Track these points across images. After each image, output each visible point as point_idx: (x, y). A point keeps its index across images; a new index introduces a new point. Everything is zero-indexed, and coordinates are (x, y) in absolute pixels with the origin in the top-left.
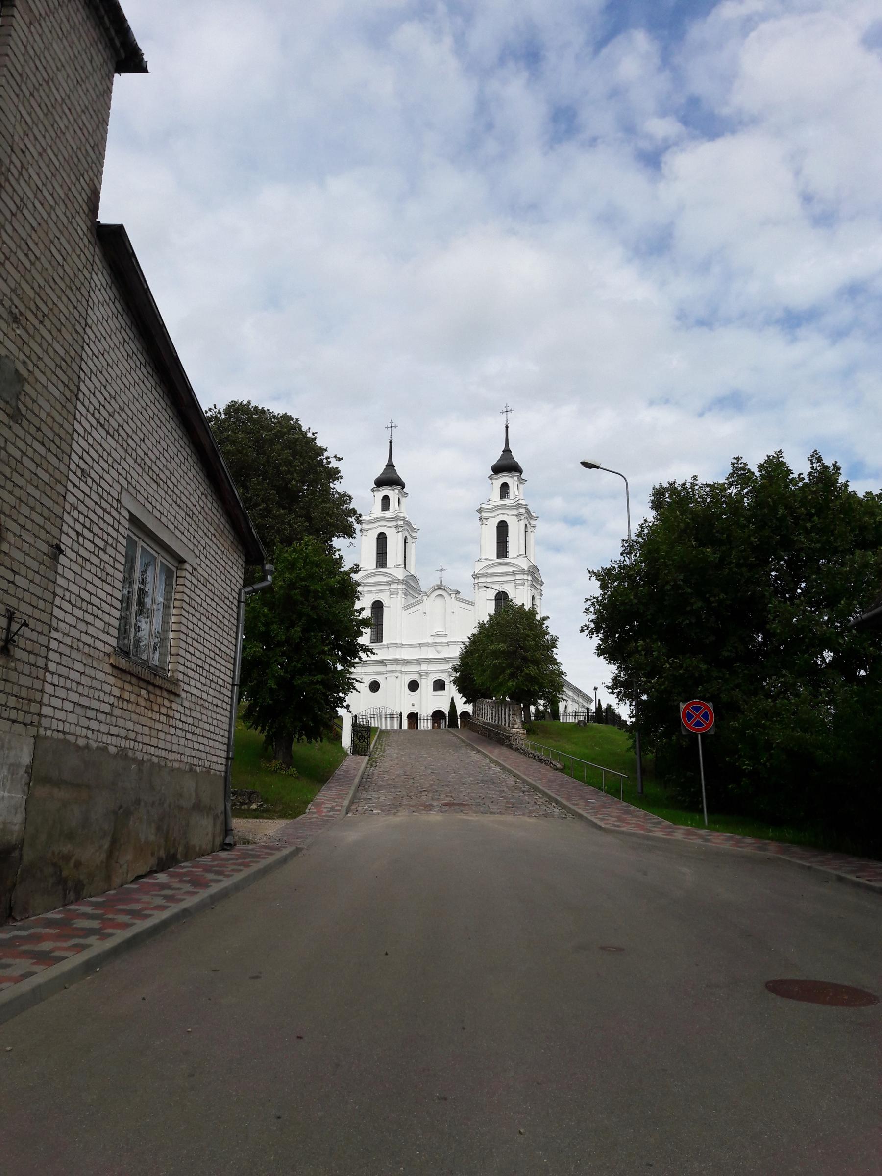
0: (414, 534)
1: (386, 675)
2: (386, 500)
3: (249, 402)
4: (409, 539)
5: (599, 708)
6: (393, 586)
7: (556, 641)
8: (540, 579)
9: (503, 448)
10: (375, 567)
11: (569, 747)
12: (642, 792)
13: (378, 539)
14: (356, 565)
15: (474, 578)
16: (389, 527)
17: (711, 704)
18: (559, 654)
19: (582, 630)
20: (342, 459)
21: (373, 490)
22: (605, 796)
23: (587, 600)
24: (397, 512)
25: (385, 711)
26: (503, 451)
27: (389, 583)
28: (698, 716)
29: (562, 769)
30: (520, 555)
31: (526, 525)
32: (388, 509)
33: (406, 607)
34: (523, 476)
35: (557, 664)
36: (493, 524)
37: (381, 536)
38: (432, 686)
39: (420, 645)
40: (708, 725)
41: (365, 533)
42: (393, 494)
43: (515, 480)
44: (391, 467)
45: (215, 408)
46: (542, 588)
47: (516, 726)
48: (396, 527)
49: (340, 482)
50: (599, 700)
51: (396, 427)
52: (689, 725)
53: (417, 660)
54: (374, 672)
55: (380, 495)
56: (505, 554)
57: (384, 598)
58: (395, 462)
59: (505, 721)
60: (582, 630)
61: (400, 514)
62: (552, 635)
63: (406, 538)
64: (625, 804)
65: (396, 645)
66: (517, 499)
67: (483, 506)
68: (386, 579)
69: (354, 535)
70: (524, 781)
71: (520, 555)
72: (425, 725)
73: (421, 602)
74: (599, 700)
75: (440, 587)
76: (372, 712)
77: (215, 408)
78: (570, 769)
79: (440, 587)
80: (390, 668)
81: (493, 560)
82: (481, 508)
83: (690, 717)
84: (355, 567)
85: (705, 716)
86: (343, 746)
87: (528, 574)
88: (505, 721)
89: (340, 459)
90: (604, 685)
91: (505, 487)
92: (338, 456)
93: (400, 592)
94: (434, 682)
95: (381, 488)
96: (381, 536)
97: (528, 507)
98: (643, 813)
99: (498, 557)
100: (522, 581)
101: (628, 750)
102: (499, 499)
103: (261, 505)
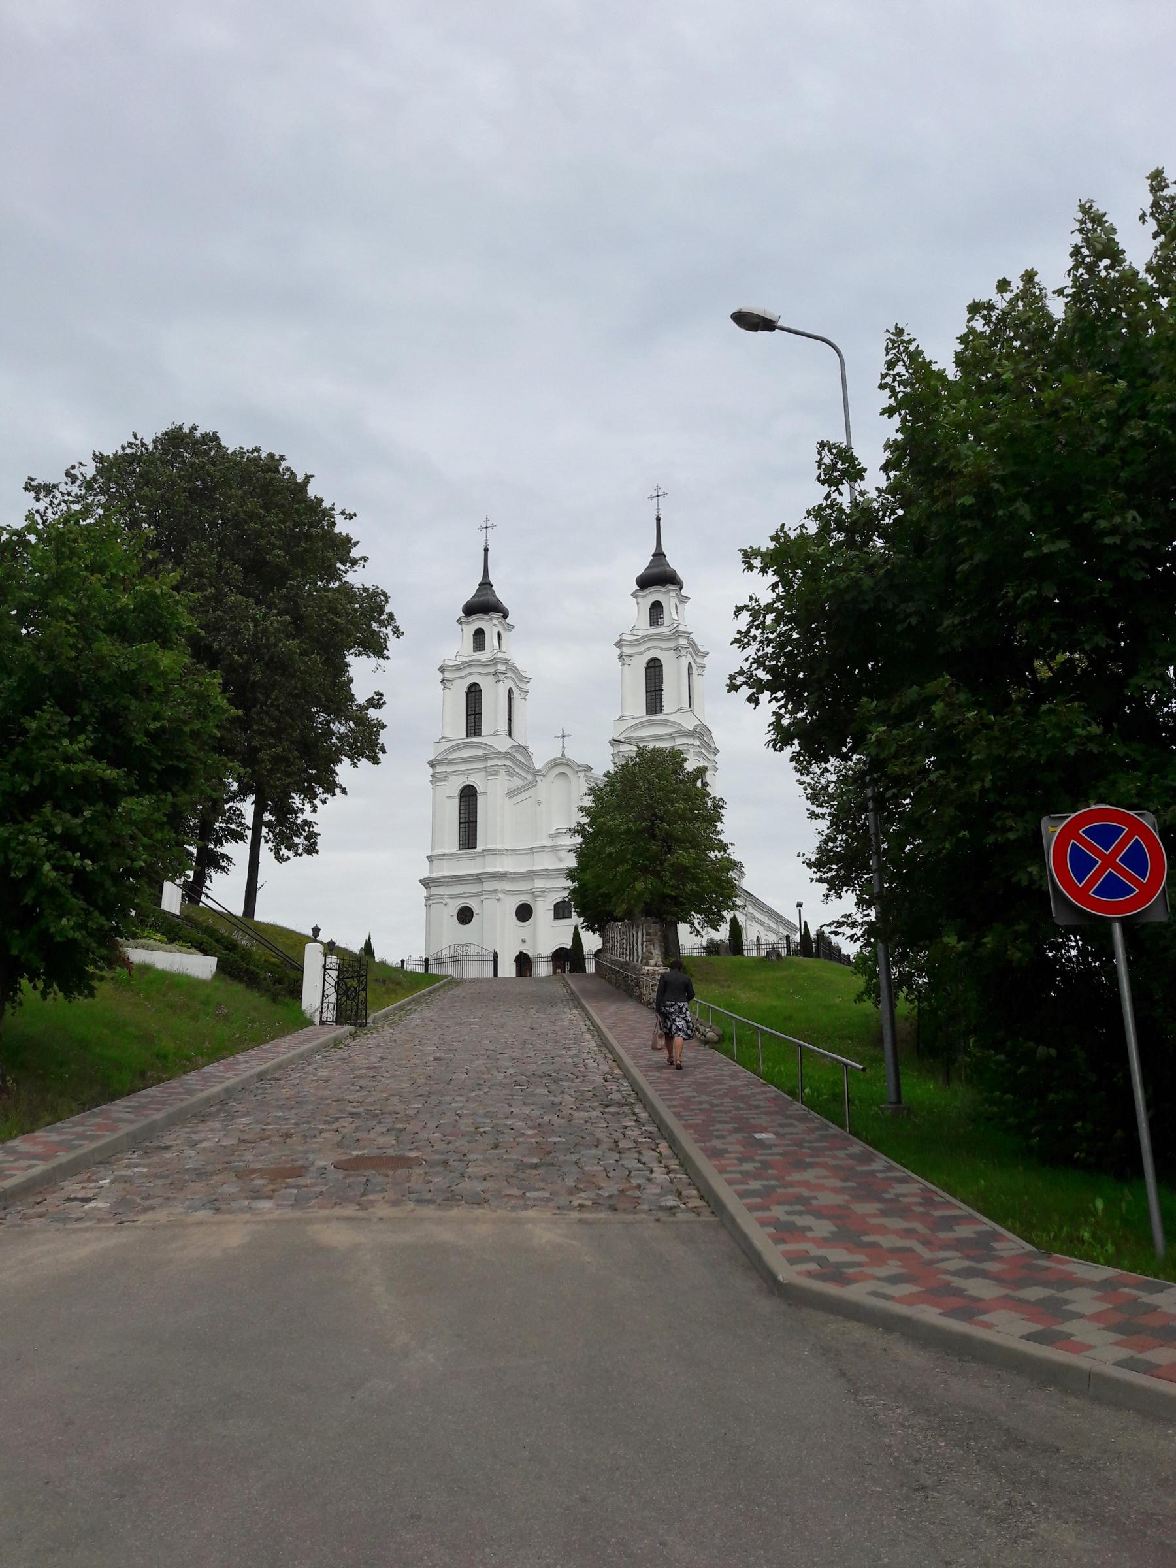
0: (522, 686)
1: (482, 898)
2: (479, 634)
3: (194, 428)
4: (516, 694)
5: (806, 935)
6: (490, 763)
7: (721, 807)
8: (713, 746)
9: (653, 550)
10: (464, 735)
11: (745, 997)
12: (899, 1101)
13: (468, 693)
14: (378, 693)
15: (612, 746)
16: (665, 650)
17: (1152, 817)
18: (730, 828)
19: (733, 687)
20: (355, 515)
21: (459, 621)
22: (802, 1119)
23: (739, 610)
24: (495, 651)
25: (472, 951)
26: (653, 556)
27: (484, 758)
28: (1108, 861)
29: (716, 1043)
30: (680, 709)
31: (690, 663)
32: (484, 649)
33: (512, 793)
34: (683, 592)
35: (723, 847)
36: (461, 687)
37: (473, 689)
38: (553, 912)
39: (533, 850)
40: (1148, 893)
41: (448, 684)
42: (491, 625)
43: (673, 597)
44: (488, 586)
45: (136, 438)
46: (716, 758)
47: (652, 962)
48: (495, 674)
49: (364, 567)
50: (805, 923)
51: (493, 526)
52: (1081, 894)
53: (528, 872)
54: (464, 893)
55: (470, 630)
56: (658, 708)
57: (477, 780)
58: (665, 549)
59: (638, 955)
60: (733, 687)
61: (500, 655)
62: (715, 798)
63: (510, 692)
64: (858, 1147)
65: (494, 851)
66: (675, 625)
67: (624, 637)
68: (480, 752)
69: (385, 652)
70: (627, 1075)
71: (680, 709)
72: (543, 970)
73: (533, 785)
74: (805, 923)
75: (561, 762)
76: (452, 952)
77: (136, 438)
78: (731, 1039)
79: (561, 762)
80: (488, 886)
81: (643, 717)
82: (621, 640)
83: (1082, 864)
84: (376, 698)
85: (1135, 859)
86: (304, 1008)
87: (694, 737)
88: (638, 955)
89: (351, 517)
90: (801, 859)
91: (656, 608)
92: (347, 512)
93: (503, 771)
94: (555, 906)
95: (473, 618)
96: (473, 689)
97: (691, 636)
98: (914, 1188)
99: (649, 712)
100: (443, 775)
101: (859, 998)
102: (649, 627)
103: (206, 590)
